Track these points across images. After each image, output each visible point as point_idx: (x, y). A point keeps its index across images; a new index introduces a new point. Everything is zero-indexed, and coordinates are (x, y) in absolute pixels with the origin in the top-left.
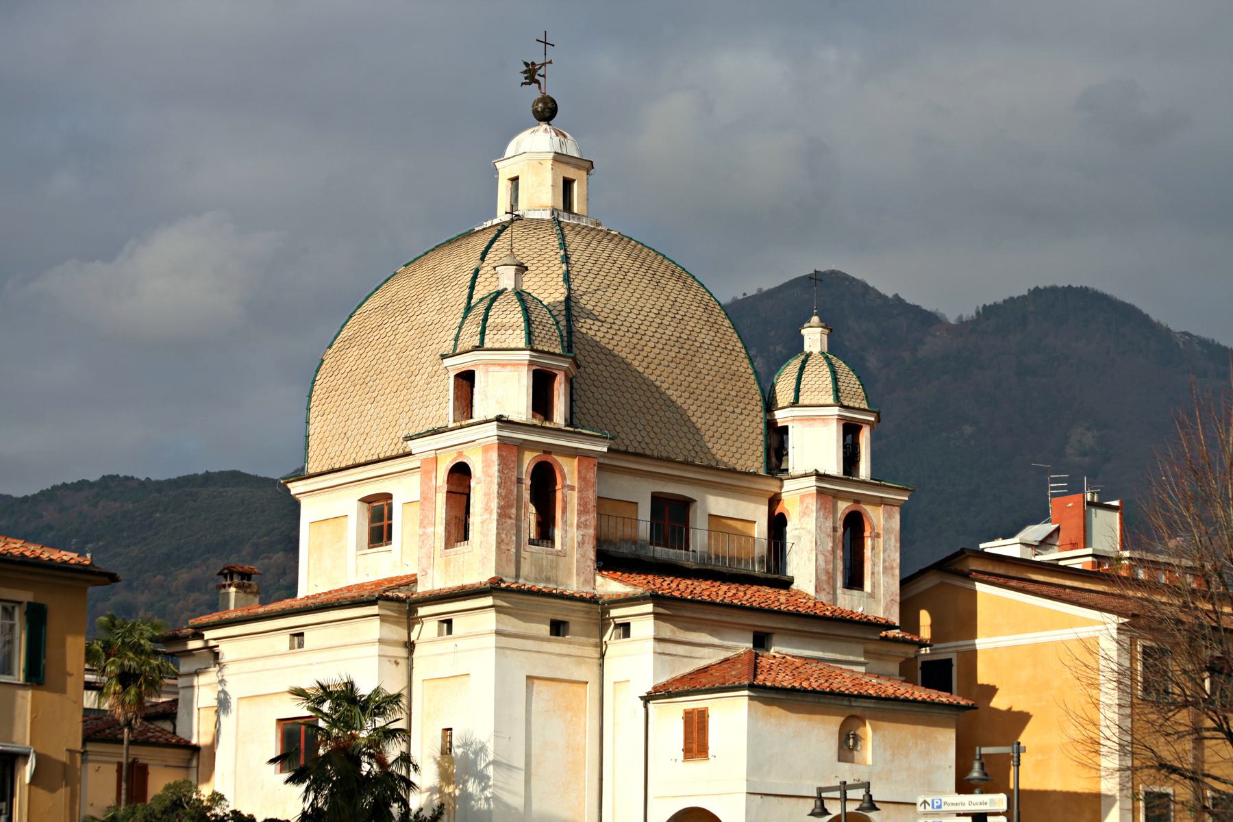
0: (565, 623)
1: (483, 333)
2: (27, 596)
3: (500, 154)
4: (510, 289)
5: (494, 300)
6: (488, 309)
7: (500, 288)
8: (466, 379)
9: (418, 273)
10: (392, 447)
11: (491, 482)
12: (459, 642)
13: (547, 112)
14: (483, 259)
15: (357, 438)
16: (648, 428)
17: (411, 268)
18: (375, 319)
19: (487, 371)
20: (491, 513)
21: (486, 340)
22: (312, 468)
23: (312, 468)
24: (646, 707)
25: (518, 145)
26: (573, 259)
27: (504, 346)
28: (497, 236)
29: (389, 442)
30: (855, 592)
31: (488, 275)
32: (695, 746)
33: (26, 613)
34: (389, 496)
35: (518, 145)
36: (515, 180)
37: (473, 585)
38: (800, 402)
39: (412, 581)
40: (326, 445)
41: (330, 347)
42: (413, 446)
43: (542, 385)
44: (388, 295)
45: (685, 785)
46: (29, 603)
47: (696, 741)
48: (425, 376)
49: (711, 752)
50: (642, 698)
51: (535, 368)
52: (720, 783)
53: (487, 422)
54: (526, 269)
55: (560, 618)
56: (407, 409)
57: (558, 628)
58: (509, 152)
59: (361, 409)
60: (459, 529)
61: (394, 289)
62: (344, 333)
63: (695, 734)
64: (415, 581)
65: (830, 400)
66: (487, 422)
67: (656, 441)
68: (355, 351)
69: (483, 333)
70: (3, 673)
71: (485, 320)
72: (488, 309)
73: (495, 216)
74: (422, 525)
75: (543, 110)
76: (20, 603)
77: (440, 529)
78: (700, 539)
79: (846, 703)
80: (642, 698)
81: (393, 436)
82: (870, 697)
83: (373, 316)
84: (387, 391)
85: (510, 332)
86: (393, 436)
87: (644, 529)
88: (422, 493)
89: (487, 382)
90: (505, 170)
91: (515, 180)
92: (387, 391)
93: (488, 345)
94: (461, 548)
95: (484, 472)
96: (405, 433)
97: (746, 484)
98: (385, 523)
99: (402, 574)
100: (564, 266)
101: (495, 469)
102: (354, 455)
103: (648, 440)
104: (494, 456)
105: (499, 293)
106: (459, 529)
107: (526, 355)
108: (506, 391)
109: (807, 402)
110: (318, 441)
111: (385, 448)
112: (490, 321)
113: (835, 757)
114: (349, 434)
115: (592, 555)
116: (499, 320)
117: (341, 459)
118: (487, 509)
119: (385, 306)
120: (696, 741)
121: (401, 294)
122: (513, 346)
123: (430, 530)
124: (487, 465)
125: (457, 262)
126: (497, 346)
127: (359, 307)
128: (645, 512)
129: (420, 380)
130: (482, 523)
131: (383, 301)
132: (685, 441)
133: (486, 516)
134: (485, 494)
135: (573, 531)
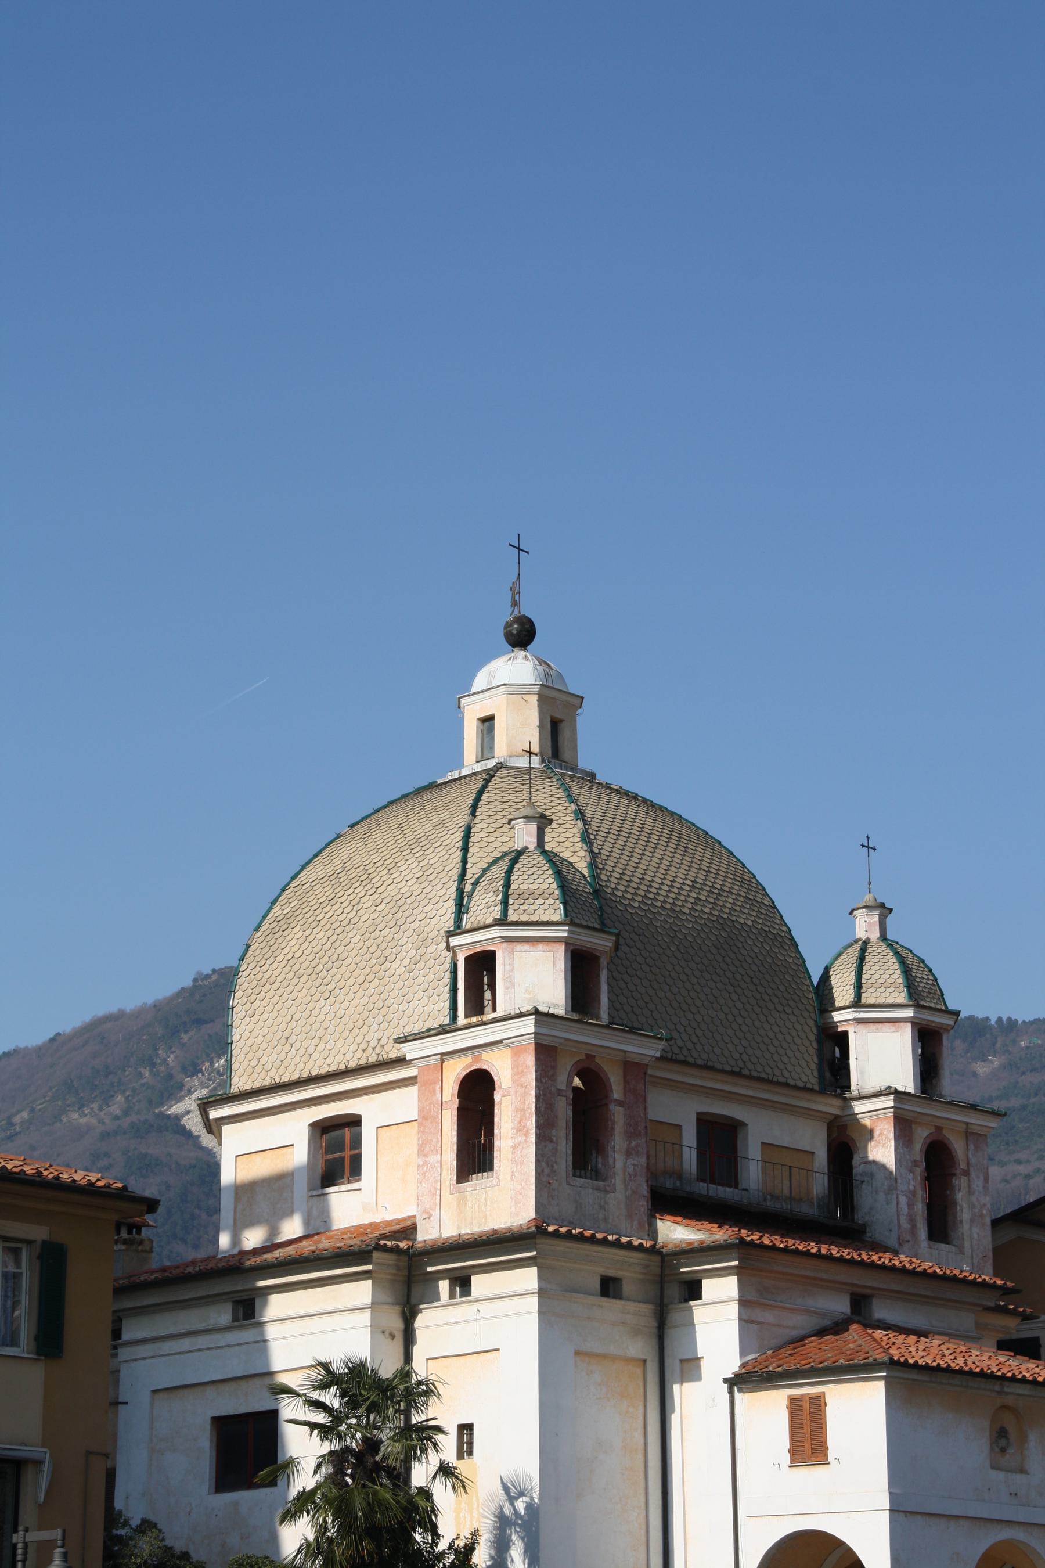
0: (616, 1281)
1: (505, 902)
2: (39, 1233)
3: (464, 687)
4: (532, 847)
5: (515, 861)
6: (509, 872)
7: (518, 846)
8: (482, 965)
9: (377, 835)
10: (359, 1054)
11: (526, 1093)
12: (481, 1306)
13: (522, 635)
14: (473, 814)
15: (305, 1044)
16: (690, 1030)
17: (363, 827)
18: (323, 893)
19: (512, 952)
20: (527, 1134)
21: (510, 912)
22: (240, 1083)
23: (240, 1083)
24: (731, 1392)
25: (491, 675)
26: (588, 813)
27: (534, 918)
28: (484, 787)
29: (353, 1048)
30: (943, 1246)
31: (483, 834)
32: (807, 1446)
33: (40, 1257)
34: (354, 1122)
35: (491, 675)
36: (488, 721)
37: (510, 1229)
38: (863, 1001)
39: (408, 1230)
40: (259, 1054)
41: (258, 928)
42: (410, 1050)
43: (581, 968)
44: (337, 862)
45: (795, 1502)
46: (44, 1242)
47: (808, 1442)
48: (406, 962)
49: (831, 1455)
50: (726, 1380)
51: (572, 948)
52: (853, 1493)
53: (521, 1015)
54: (551, 821)
55: (612, 1273)
56: (380, 1004)
57: (609, 1287)
58: (480, 682)
59: (312, 1004)
60: (475, 1155)
61: (344, 854)
62: (277, 910)
63: (807, 1429)
64: (413, 1228)
65: (902, 998)
66: (521, 1015)
67: (699, 1047)
68: (298, 933)
69: (505, 902)
70: (4, 1344)
71: (507, 885)
72: (509, 872)
73: (461, 765)
74: (422, 1151)
75: (520, 632)
76: (29, 1242)
77: (450, 1157)
78: (753, 1173)
79: (997, 1388)
80: (726, 1380)
81: (359, 1039)
82: (1024, 1381)
83: (318, 889)
84: (350, 982)
85: (540, 901)
86: (359, 1039)
87: (690, 1158)
88: (421, 1111)
89: (512, 965)
90: (473, 710)
91: (488, 721)
92: (350, 982)
93: (513, 917)
94: (478, 1182)
95: (514, 1081)
96: (399, 1033)
97: (805, 1105)
98: (348, 1153)
99: (367, 1222)
100: (580, 823)
101: (530, 1077)
102: (301, 1066)
103: (689, 1045)
104: (529, 1060)
105: (520, 853)
106: (475, 1155)
107: (563, 932)
108: (535, 978)
109: (871, 1001)
110: (246, 1050)
111: (319, 1063)
112: (513, 887)
113: (786, 1458)
114: (292, 1040)
115: (644, 1190)
116: (524, 887)
117: (281, 1071)
118: (521, 1129)
119: (334, 876)
120: (808, 1442)
121: (357, 860)
122: (545, 919)
123: (434, 1159)
124: (518, 1072)
125: (435, 819)
126: (524, 918)
127: (294, 878)
128: (690, 1137)
129: (398, 968)
130: (514, 1147)
131: (330, 869)
132: (731, 1047)
133: (520, 1138)
134: (517, 1110)
135: (623, 1160)
